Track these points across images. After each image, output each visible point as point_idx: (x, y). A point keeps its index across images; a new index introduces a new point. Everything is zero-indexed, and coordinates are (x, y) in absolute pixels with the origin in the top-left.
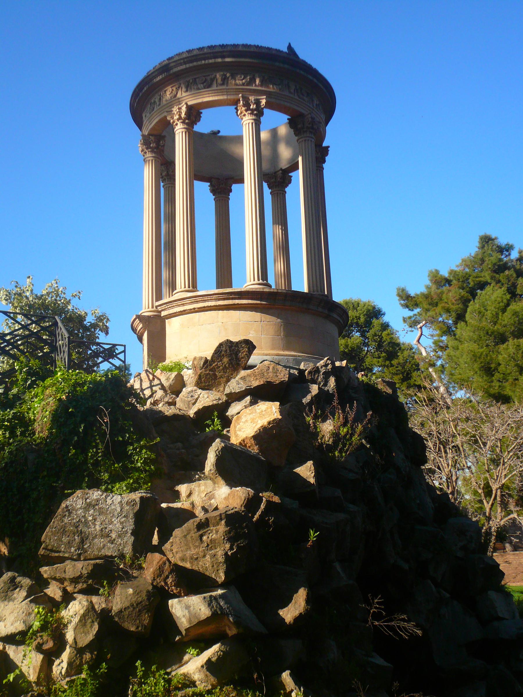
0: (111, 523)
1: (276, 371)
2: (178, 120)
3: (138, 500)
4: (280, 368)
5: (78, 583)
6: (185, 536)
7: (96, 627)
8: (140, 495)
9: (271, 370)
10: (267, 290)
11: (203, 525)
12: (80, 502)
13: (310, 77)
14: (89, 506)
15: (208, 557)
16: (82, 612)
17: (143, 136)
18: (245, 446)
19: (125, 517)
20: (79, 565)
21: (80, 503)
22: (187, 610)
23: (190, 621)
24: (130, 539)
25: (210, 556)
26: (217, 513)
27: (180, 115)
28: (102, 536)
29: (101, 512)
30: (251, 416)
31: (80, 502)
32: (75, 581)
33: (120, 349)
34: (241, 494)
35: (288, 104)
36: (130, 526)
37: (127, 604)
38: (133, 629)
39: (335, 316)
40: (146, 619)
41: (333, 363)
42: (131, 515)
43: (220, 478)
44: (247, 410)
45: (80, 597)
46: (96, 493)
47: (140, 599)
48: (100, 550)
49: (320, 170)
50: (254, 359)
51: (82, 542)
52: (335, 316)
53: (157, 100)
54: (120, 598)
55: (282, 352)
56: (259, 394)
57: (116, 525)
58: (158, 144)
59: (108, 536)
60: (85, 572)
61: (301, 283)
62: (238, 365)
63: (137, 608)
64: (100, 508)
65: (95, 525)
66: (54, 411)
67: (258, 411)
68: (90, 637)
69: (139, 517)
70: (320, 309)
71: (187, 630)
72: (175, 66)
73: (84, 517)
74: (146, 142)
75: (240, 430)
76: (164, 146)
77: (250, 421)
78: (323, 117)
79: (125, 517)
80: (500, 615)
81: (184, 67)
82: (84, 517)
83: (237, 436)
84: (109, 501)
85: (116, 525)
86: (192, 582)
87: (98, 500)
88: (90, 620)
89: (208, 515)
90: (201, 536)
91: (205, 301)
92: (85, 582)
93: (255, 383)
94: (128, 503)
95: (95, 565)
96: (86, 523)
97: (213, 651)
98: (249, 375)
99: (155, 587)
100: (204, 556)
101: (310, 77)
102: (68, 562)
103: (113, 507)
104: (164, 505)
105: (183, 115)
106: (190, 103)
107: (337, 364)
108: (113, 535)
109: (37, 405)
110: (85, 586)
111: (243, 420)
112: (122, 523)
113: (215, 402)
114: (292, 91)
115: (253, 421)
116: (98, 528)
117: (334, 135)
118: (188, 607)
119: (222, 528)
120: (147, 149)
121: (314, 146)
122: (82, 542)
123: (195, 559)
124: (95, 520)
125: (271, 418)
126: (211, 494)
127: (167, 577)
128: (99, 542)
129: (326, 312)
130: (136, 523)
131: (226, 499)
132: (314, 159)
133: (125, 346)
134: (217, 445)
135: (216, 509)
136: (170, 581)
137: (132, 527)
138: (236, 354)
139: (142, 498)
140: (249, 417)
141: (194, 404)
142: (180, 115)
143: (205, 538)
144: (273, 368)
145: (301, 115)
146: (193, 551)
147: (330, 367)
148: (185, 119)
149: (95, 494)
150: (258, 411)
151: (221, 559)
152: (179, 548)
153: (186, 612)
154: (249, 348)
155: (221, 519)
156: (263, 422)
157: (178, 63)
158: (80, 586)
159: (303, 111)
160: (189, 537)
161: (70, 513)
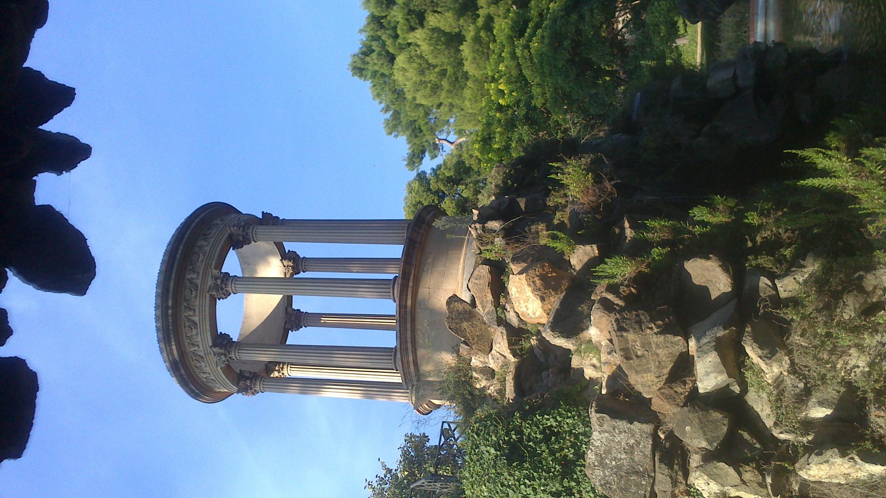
0: (619, 443)
1: (479, 277)
2: (226, 356)
3: (598, 415)
4: (476, 272)
5: (677, 479)
6: (637, 372)
7: (722, 465)
8: (593, 413)
9: (477, 282)
10: (399, 281)
11: (627, 355)
12: (597, 472)
13: (194, 225)
14: (602, 464)
15: (659, 351)
16: (706, 477)
17: (238, 392)
18: (550, 310)
19: (614, 429)
20: (659, 477)
21: (599, 472)
22: (709, 376)
23: (720, 372)
24: (637, 426)
25: (659, 347)
26: (615, 340)
27: (221, 354)
28: (632, 453)
29: (608, 452)
30: (522, 302)
31: (597, 472)
32: (675, 483)
33: (446, 426)
34: (597, 316)
35: (220, 247)
36: (623, 424)
37: (701, 432)
38: (725, 429)
39: (429, 217)
40: (717, 415)
41: (475, 222)
42: (613, 423)
43: (581, 335)
44: (516, 305)
45: (692, 479)
46: (590, 456)
47: (697, 420)
48: (645, 456)
49: (285, 222)
50: (466, 297)
51: (637, 473)
52: (429, 217)
53: (204, 376)
54: (696, 441)
55: (461, 266)
56: (499, 289)
57: (622, 439)
58: (247, 378)
59: (632, 447)
60: (666, 471)
61: (396, 251)
62: (470, 312)
63: (704, 427)
64: (604, 453)
65: (621, 459)
66: (561, 11)
67: (517, 295)
68: (731, 471)
69: (615, 415)
70: (422, 231)
71: (730, 376)
72: (172, 354)
73: (612, 469)
74: (245, 390)
75: (535, 314)
76: (250, 373)
77: (528, 302)
78: (233, 215)
79: (614, 429)
80: (731, 75)
81: (174, 347)
82: (612, 469)
83: (540, 317)
84: (598, 443)
85: (622, 439)
86: (683, 368)
87: (596, 455)
88: (715, 470)
89: (617, 350)
90: (637, 356)
91: (406, 341)
92: (676, 472)
93: (490, 297)
94: (601, 425)
95: (661, 461)
96: (619, 468)
97: (753, 353)
98: (481, 303)
99: (685, 405)
100: (657, 355)
101: (194, 225)
102: (656, 489)
103: (604, 440)
104: (604, 392)
105: (222, 351)
106: (211, 344)
107: (475, 218)
108: (632, 441)
109: (521, 308)
110: (680, 473)
111: (524, 309)
112: (620, 433)
113: (505, 337)
114: (206, 244)
115: (527, 300)
116: (623, 456)
117: (249, 205)
118: (707, 374)
119: (631, 336)
120: (251, 389)
121: (261, 227)
122: (637, 473)
123: (660, 366)
124: (615, 458)
125: (524, 282)
126: (596, 351)
127: (676, 392)
128: (638, 456)
129: (424, 226)
130: (621, 419)
131: (601, 331)
132: (274, 227)
133: (443, 422)
134: (548, 336)
135: (611, 341)
136: (679, 390)
137: (625, 423)
138: (460, 313)
139: (597, 412)
140: (523, 305)
141: (505, 357)
142: (221, 354)
143: (639, 353)
144: (476, 279)
145: (231, 236)
146: (652, 366)
147: (478, 226)
148: (225, 350)
149: (591, 457)
150: (517, 295)
151: (661, 338)
152: (647, 382)
153: (712, 375)
154: (455, 301)
155: (622, 336)
156: (528, 291)
157: (170, 353)
158: (680, 478)
159: (227, 235)
160: (638, 369)
161: (607, 483)
